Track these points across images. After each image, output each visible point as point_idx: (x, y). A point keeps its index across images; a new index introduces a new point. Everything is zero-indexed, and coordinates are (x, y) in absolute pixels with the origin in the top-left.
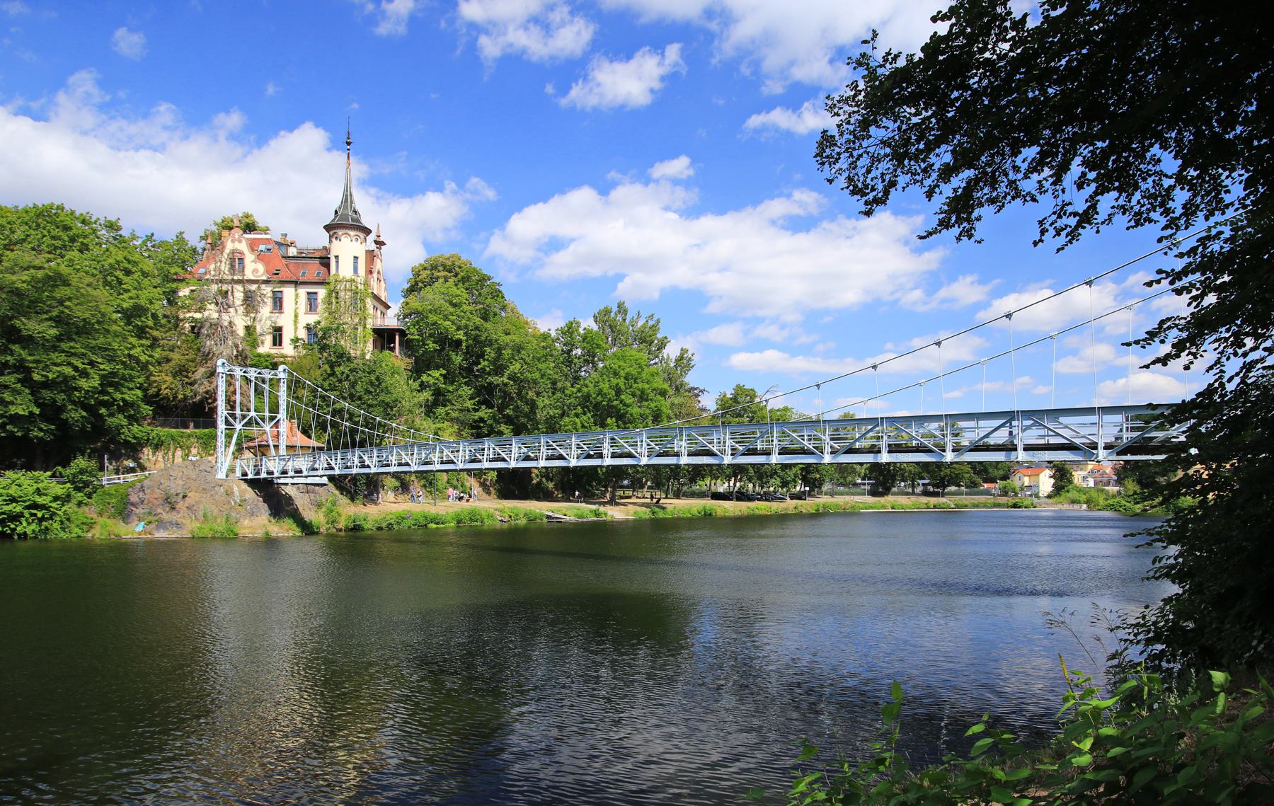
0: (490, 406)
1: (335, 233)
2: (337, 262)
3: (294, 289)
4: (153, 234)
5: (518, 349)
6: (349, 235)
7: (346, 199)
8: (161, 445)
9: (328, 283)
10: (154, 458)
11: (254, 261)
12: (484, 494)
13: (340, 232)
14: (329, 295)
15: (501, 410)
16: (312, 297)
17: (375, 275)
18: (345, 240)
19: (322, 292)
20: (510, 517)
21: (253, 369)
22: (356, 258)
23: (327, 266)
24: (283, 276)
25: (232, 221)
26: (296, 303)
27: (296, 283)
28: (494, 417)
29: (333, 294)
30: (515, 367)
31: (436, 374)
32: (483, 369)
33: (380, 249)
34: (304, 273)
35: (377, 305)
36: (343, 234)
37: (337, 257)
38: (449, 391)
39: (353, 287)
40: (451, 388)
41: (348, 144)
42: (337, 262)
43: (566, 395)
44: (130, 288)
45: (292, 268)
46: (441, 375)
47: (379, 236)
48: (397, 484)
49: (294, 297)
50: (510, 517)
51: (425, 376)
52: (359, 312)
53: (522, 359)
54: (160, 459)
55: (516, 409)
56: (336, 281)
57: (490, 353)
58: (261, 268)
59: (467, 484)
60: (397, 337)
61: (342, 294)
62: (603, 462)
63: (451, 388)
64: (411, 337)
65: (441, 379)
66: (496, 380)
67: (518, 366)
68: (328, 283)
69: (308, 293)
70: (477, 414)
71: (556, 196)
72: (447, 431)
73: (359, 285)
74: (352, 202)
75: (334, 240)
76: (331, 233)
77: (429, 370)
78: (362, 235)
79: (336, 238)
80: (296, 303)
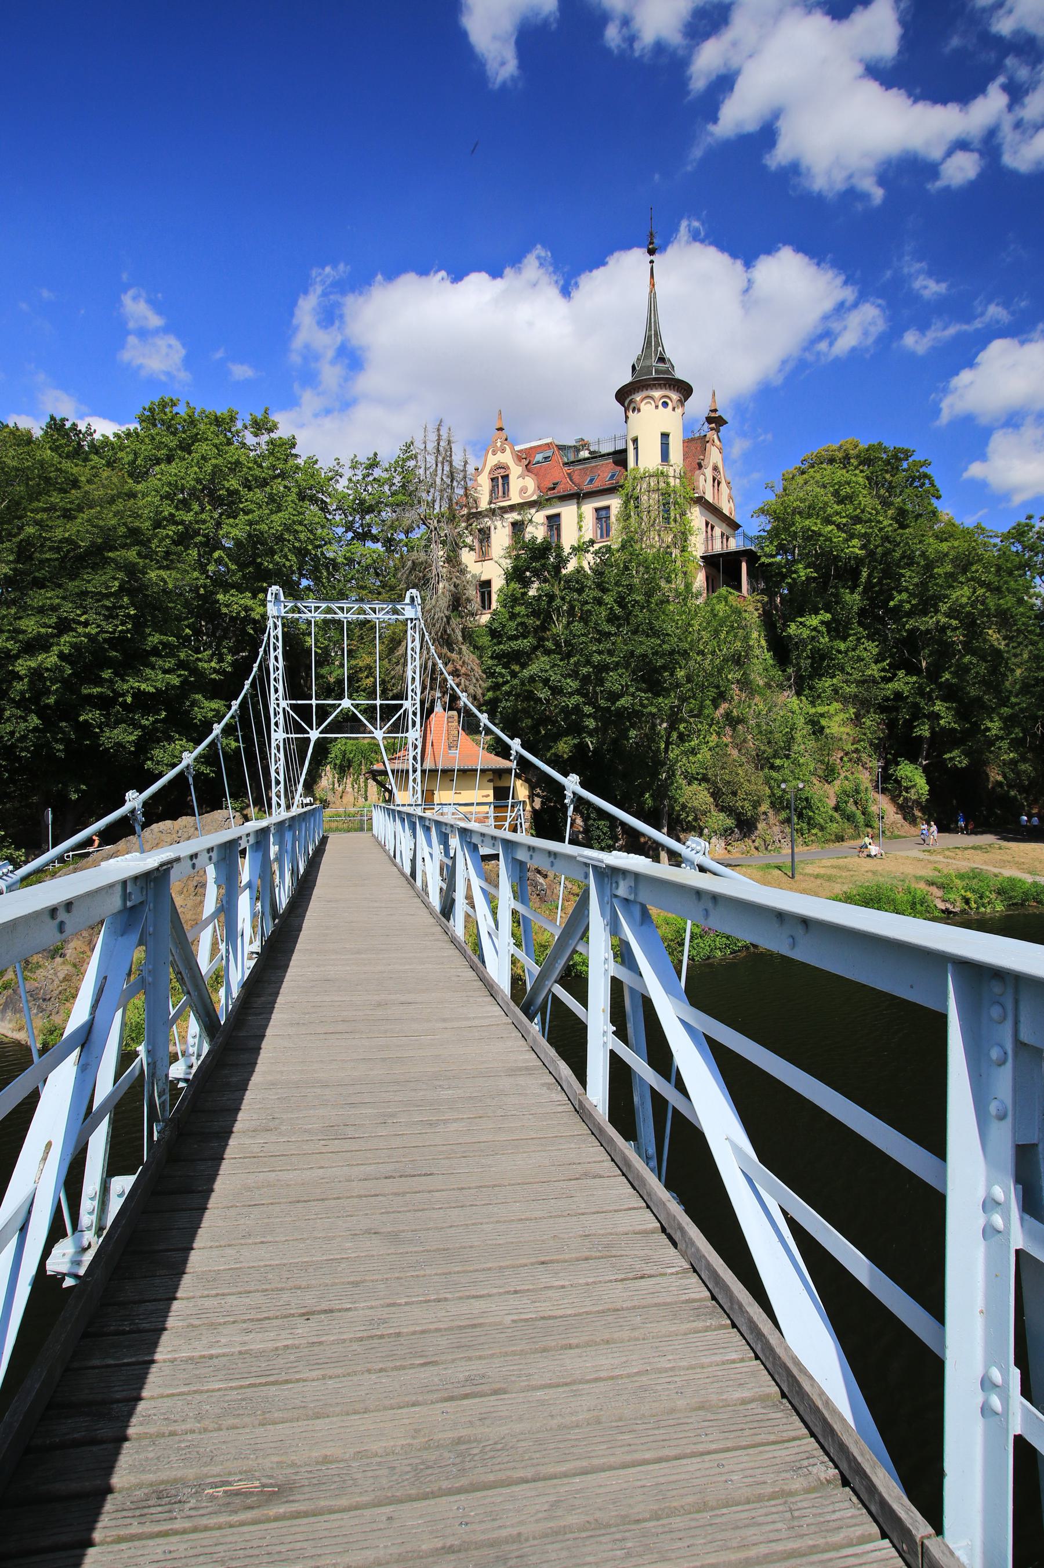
0: (913, 669)
1: (631, 402)
2: (636, 449)
3: (575, 507)
4: (376, 454)
5: (964, 564)
8: (349, 767)
9: (621, 486)
10: (340, 789)
11: (521, 476)
12: (906, 824)
13: (638, 397)
14: (626, 504)
15: (933, 674)
16: (602, 515)
17: (709, 472)
19: (615, 503)
20: (967, 901)
22: (665, 436)
24: (560, 490)
26: (580, 529)
27: (579, 497)
28: (920, 691)
29: (632, 500)
30: (962, 594)
31: (814, 621)
32: (898, 607)
33: (718, 431)
34: (591, 481)
35: (713, 520)
37: (635, 441)
38: (839, 652)
39: (662, 485)
40: (842, 646)
42: (636, 449)
44: (253, 507)
46: (822, 623)
48: (730, 822)
50: (967, 901)
51: (793, 626)
52: (672, 524)
53: (973, 579)
54: (349, 789)
55: (962, 671)
57: (910, 577)
58: (530, 483)
59: (873, 809)
60: (744, 565)
61: (644, 498)
63: (842, 646)
64: (767, 561)
65: (823, 629)
66: (927, 622)
67: (966, 591)
69: (597, 510)
70: (890, 685)
72: (836, 718)
73: (671, 481)
74: (657, 345)
75: (630, 414)
77: (802, 616)
78: (675, 396)
80: (580, 529)
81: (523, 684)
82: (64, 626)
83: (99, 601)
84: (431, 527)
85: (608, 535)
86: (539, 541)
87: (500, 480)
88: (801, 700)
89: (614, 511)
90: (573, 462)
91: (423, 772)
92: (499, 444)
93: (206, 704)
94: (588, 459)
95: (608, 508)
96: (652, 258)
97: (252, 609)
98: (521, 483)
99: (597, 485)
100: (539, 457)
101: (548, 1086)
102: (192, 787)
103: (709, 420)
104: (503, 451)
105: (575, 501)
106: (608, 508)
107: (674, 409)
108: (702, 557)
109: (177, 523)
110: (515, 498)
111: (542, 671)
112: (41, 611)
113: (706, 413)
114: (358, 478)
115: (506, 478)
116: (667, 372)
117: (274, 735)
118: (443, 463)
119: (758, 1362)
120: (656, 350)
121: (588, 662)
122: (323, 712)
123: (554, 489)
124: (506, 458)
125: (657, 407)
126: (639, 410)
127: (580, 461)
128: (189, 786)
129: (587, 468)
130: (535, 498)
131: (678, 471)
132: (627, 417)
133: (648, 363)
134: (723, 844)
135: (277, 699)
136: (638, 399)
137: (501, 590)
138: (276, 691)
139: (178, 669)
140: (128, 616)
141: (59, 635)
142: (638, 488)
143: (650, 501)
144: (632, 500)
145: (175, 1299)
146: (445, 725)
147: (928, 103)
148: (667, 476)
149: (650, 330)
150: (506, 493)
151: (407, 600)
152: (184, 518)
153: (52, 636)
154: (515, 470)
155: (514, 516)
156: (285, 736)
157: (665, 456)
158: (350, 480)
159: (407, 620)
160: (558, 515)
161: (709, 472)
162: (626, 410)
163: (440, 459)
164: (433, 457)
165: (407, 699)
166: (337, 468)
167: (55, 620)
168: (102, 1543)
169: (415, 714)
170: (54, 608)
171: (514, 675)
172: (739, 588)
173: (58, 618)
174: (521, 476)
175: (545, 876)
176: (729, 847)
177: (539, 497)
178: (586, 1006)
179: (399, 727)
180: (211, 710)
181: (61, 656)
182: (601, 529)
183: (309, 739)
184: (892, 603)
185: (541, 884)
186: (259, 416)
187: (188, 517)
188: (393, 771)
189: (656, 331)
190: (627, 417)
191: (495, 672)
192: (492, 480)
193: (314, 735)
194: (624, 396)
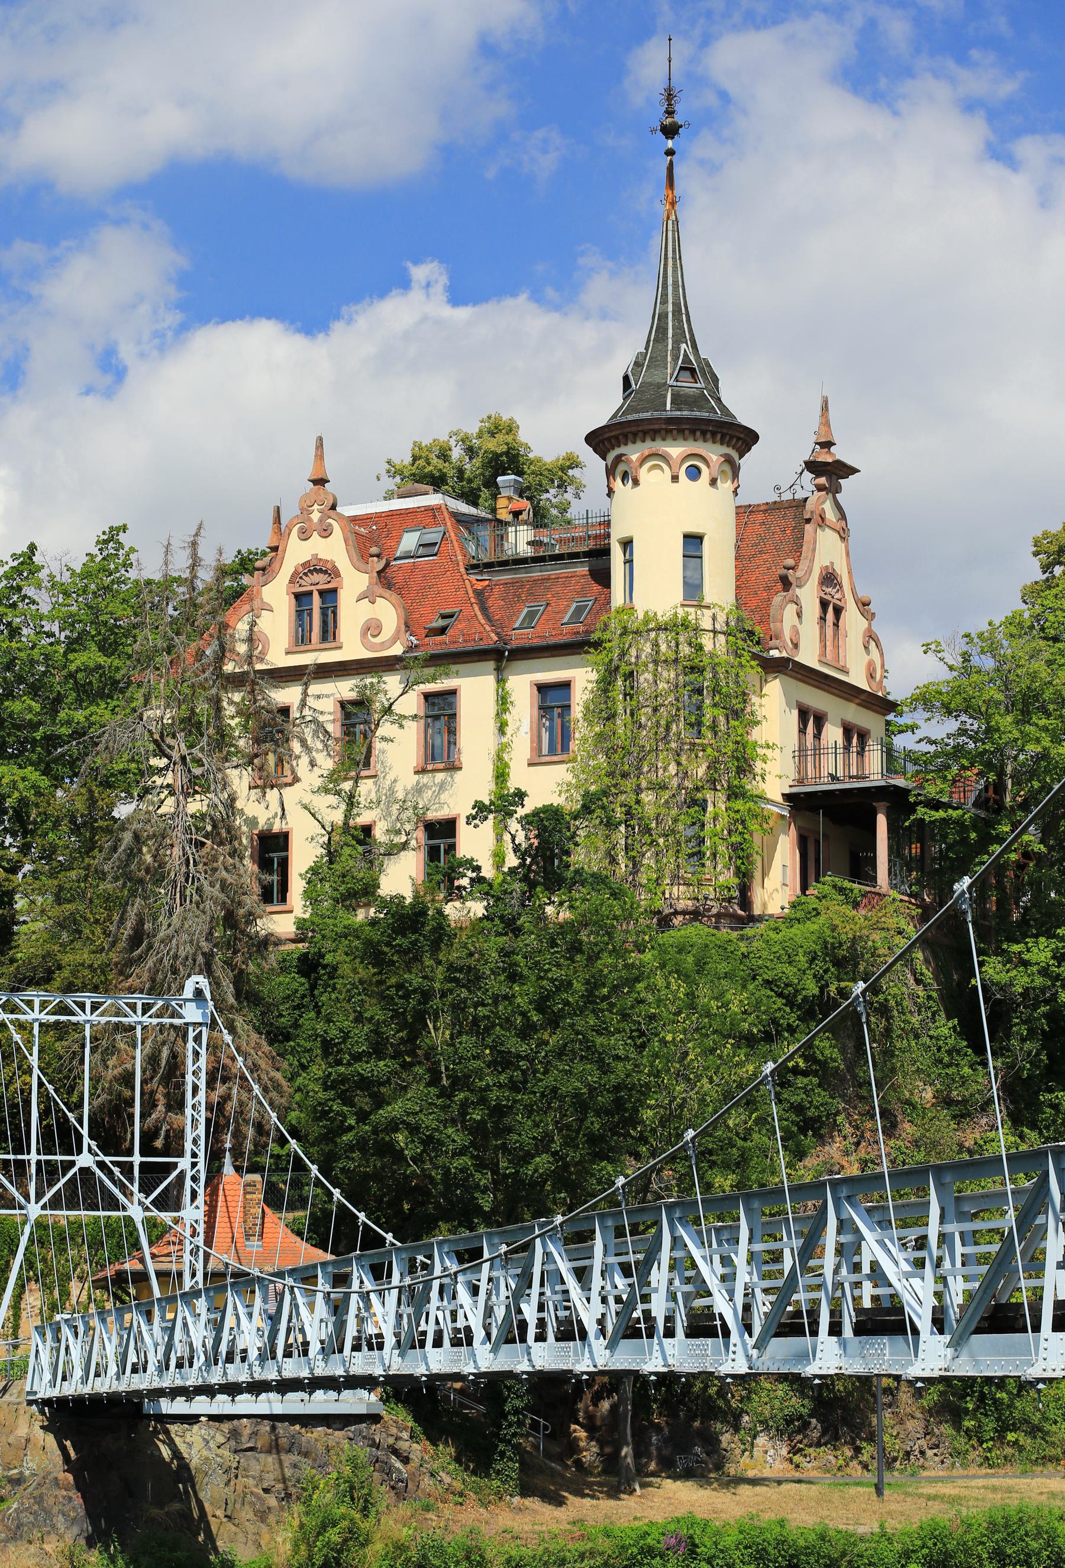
1: (619, 459)
2: (629, 562)
4: (32, 548)
6: (665, 458)
7: (661, 330)
9: (597, 645)
13: (634, 453)
14: (605, 684)
18: (654, 478)
21: (36, 995)
22: (693, 541)
23: (602, 577)
24: (456, 639)
25: (444, 456)
26: (502, 730)
35: (817, 699)
36: (643, 461)
37: (627, 544)
39: (685, 650)
41: (670, 131)
42: (629, 562)
43: (854, 1076)
45: (495, 602)
47: (827, 445)
49: (492, 708)
56: (625, 632)
60: (882, 821)
61: (645, 678)
62: (805, 1357)
68: (597, 645)
69: (542, 689)
71: (394, 292)
73: (707, 641)
76: (611, 456)
78: (714, 453)
79: (625, 476)
80: (502, 730)
81: (375, 1131)
84: (176, 756)
85: (565, 748)
86: (408, 901)
87: (316, 598)
88: (1022, 1137)
89: (581, 696)
90: (489, 565)
91: (205, 1275)
92: (316, 516)
94: (524, 561)
95: (566, 685)
96: (670, 144)
98: (365, 611)
100: (409, 541)
103: (813, 467)
105: (491, 665)
106: (566, 685)
107: (713, 482)
108: (787, 797)
111: (408, 1114)
115: (330, 595)
116: (698, 401)
120: (676, 349)
121: (483, 1101)
123: (442, 631)
125: (675, 478)
126: (636, 482)
127: (504, 563)
130: (397, 650)
131: (721, 618)
132: (610, 493)
133: (658, 379)
134: (784, 1451)
136: (634, 457)
137: (314, 870)
142: (633, 652)
146: (241, 1198)
148: (697, 629)
149: (664, 302)
150: (329, 633)
155: (346, 688)
157: (693, 589)
159: (187, 1024)
160: (453, 692)
161: (809, 594)
162: (610, 472)
169: (194, 1179)
171: (363, 1117)
172: (872, 879)
175: (406, 1460)
176: (797, 1458)
177: (410, 649)
179: (169, 1201)
182: (551, 730)
185: (399, 1471)
188: (159, 1274)
189: (677, 305)
190: (610, 493)
191: (331, 1110)
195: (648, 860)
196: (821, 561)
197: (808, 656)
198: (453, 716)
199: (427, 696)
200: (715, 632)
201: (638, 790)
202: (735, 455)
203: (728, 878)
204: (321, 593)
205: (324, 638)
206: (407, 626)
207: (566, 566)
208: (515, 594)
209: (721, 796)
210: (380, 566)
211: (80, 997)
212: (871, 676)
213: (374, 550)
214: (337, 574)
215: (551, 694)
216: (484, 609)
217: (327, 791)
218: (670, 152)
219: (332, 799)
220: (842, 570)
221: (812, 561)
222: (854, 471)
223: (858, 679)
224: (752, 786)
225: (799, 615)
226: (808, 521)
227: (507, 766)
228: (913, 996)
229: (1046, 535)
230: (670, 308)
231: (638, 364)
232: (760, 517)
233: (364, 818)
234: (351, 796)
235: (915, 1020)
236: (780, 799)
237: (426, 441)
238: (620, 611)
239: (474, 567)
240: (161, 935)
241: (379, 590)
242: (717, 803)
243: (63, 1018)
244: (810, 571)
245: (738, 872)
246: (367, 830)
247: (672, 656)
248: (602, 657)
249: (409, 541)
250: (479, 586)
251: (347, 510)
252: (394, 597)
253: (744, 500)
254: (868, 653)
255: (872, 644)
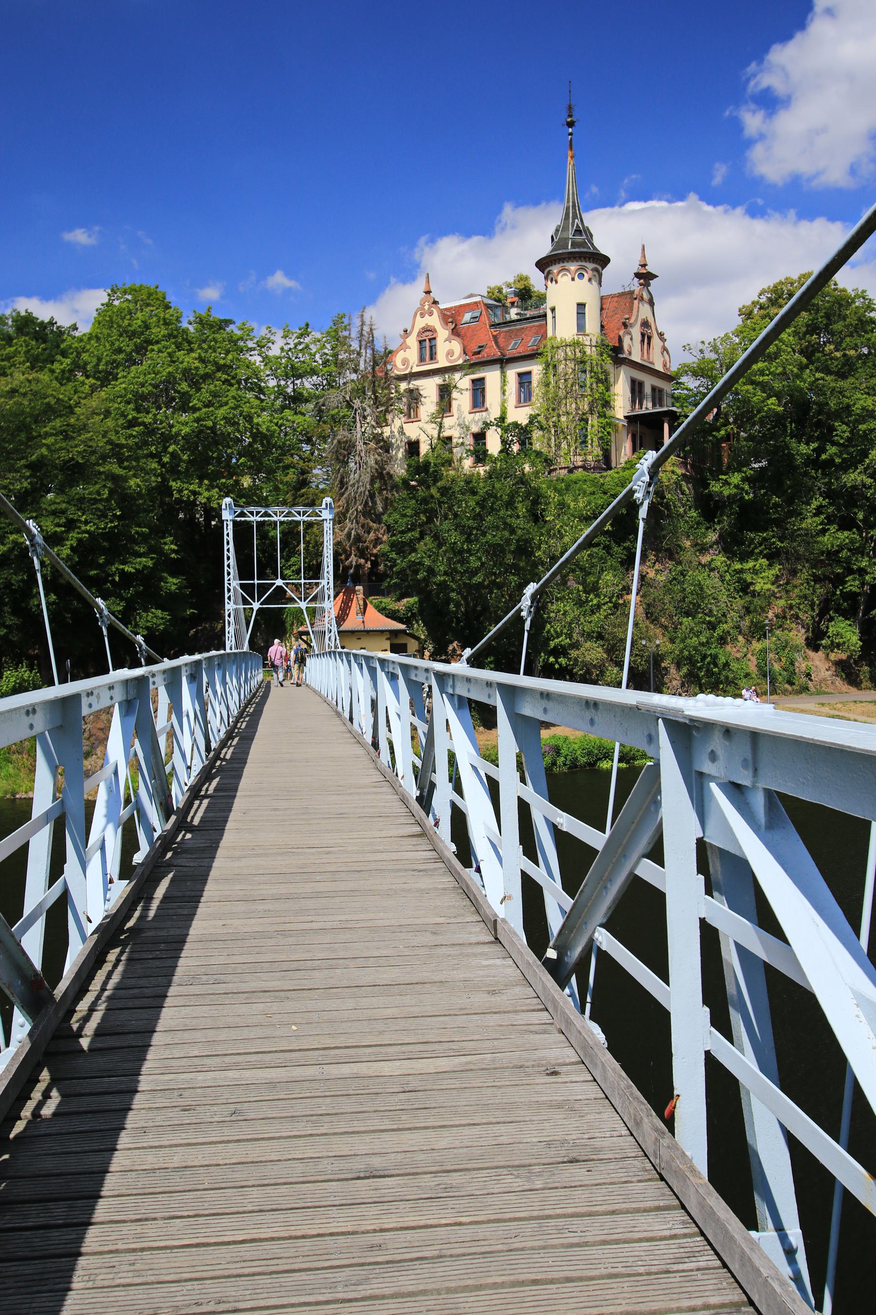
1: (549, 273)
2: (554, 317)
6: (568, 270)
7: (567, 214)
9: (540, 354)
11: (448, 340)
13: (555, 269)
16: (524, 379)
19: (536, 369)
24: (484, 356)
26: (504, 393)
27: (503, 362)
36: (559, 272)
37: (553, 310)
39: (579, 355)
42: (554, 317)
45: (501, 340)
56: (553, 347)
58: (456, 346)
61: (561, 368)
68: (540, 354)
69: (520, 375)
73: (588, 350)
76: (546, 272)
78: (590, 266)
79: (552, 281)
80: (504, 393)
82: (71, 525)
83: (94, 504)
85: (530, 400)
89: (536, 378)
92: (426, 307)
93: (170, 580)
94: (513, 321)
95: (529, 373)
96: (570, 130)
97: (200, 494)
99: (521, 351)
100: (467, 317)
101: (683, 1222)
102: (106, 639)
103: (638, 275)
104: (431, 314)
105: (498, 366)
107: (590, 280)
108: (626, 417)
109: (139, 424)
110: (442, 362)
112: (54, 513)
113: (636, 268)
114: (289, 346)
116: (583, 244)
117: (227, 607)
118: (366, 348)
119: (725, 1270)
120: (573, 222)
122: (263, 589)
123: (479, 353)
124: (434, 321)
125: (573, 279)
126: (556, 282)
128: (103, 637)
129: (512, 331)
130: (460, 362)
133: (565, 236)
135: (229, 580)
138: (229, 574)
139: (149, 554)
140: (115, 515)
141: (67, 532)
143: (566, 368)
144: (551, 367)
145: (80, 1254)
147: (810, 16)
150: (433, 357)
151: (324, 506)
152: (145, 420)
153: (62, 532)
154: (443, 333)
155: (438, 380)
156: (235, 606)
157: (581, 327)
158: (282, 349)
161: (636, 331)
162: (546, 278)
163: (363, 343)
164: (357, 342)
165: (323, 578)
166: (268, 336)
167: (63, 520)
168: (121, 1150)
170: (63, 512)
173: (66, 518)
174: (448, 340)
177: (465, 361)
178: (666, 978)
180: (174, 584)
181: (72, 548)
183: (252, 609)
184: (824, 457)
186: (204, 314)
187: (148, 419)
189: (574, 203)
192: (421, 342)
193: (256, 606)
194: (543, 264)
195: (564, 445)
196: (642, 316)
197: (636, 357)
198: (483, 389)
199: (473, 381)
200: (591, 346)
201: (559, 416)
202: (600, 268)
203: (598, 451)
204: (430, 340)
205: (431, 359)
206: (465, 353)
207: (530, 322)
208: (510, 336)
209: (595, 417)
210: (453, 326)
211: (252, 509)
212: (665, 366)
213: (450, 320)
214: (436, 331)
215: (524, 377)
216: (496, 343)
217: (432, 422)
218: (571, 134)
219: (434, 425)
220: (651, 320)
221: (637, 316)
222: (656, 276)
223: (659, 367)
224: (609, 413)
225: (631, 339)
226: (636, 299)
227: (506, 408)
228: (680, 500)
229: (744, 307)
230: (571, 204)
231: (557, 230)
232: (616, 299)
233: (446, 434)
234: (441, 424)
235: (682, 510)
236: (622, 418)
237: (492, 286)
238: (551, 339)
239: (493, 325)
240: (351, 483)
241: (453, 337)
242: (594, 421)
243: (266, 519)
244: (636, 320)
245: (602, 449)
246: (450, 439)
247: (573, 357)
248: (543, 360)
249: (467, 317)
250: (495, 333)
251: (442, 306)
252: (459, 339)
253: (606, 290)
254: (663, 357)
255: (665, 353)
